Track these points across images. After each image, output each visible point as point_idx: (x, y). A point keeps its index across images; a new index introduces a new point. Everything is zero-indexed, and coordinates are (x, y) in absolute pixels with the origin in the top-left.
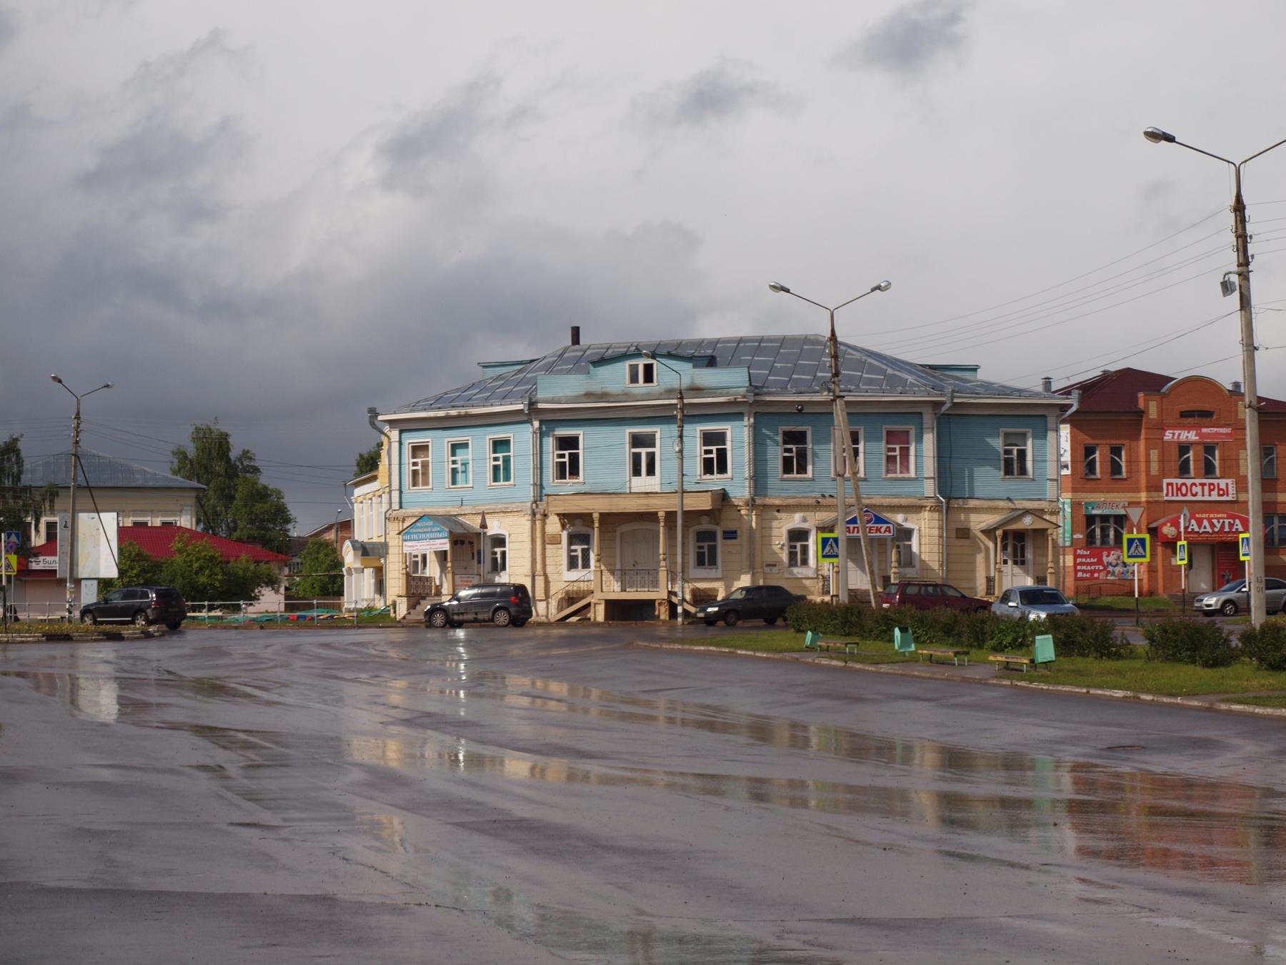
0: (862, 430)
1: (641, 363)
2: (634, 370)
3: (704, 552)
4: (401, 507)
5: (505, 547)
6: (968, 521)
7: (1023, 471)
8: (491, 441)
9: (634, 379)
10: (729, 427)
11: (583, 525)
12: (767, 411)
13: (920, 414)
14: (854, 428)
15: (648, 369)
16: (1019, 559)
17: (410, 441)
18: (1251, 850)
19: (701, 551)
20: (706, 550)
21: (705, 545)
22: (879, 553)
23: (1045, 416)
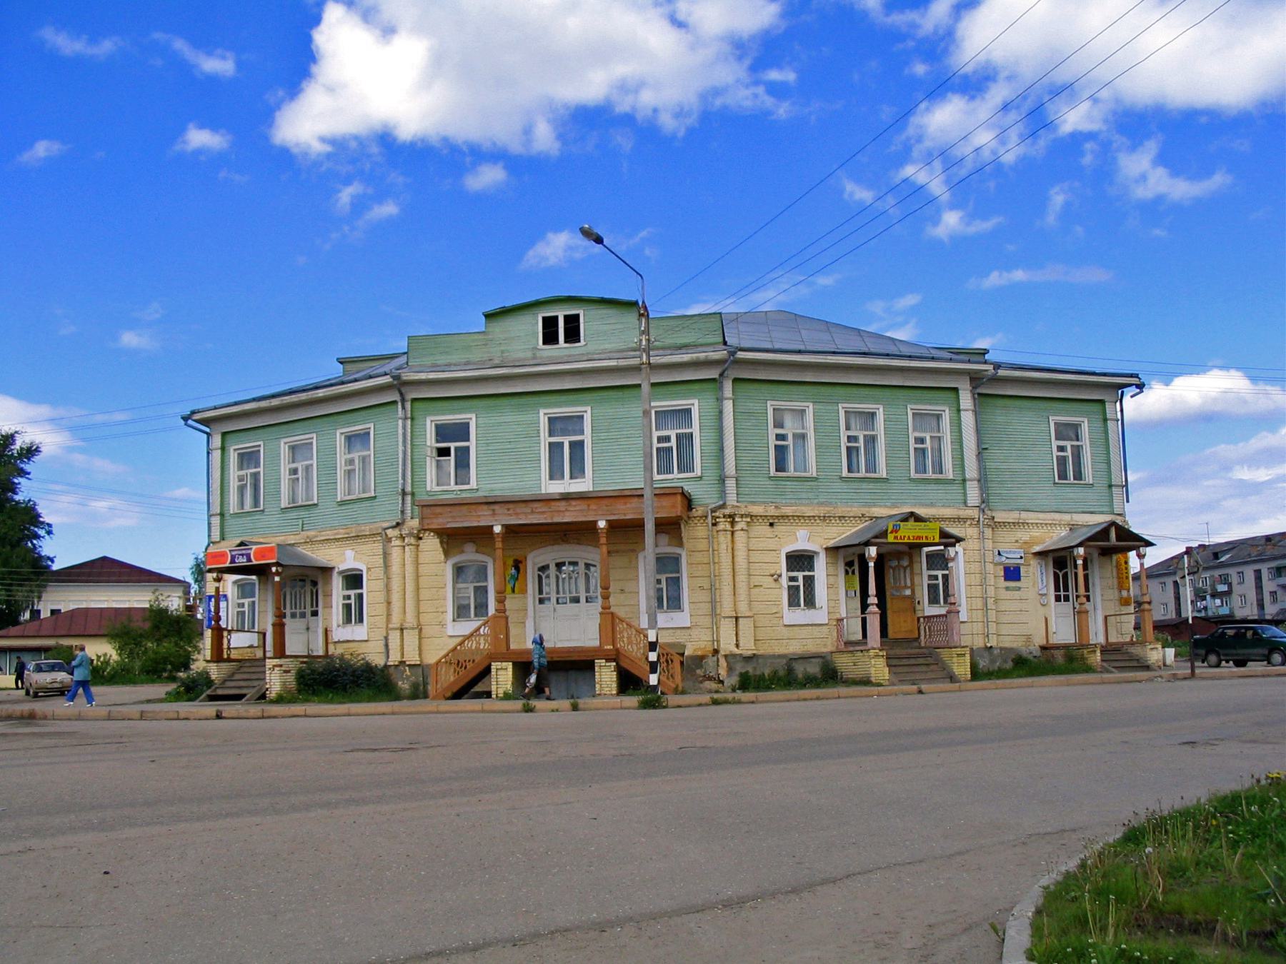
0: (881, 410)
1: (561, 313)
2: (550, 324)
3: (799, 586)
4: (223, 539)
5: (361, 587)
6: (113, 660)
7: (1078, 475)
8: (343, 437)
9: (550, 338)
10: (696, 402)
11: (477, 552)
12: (741, 377)
13: (956, 390)
14: (659, 577)
15: (572, 322)
16: (1062, 593)
17: (236, 447)
18: (800, 669)
19: (1062, 454)
20: (801, 582)
21: (800, 575)
22: (1100, 578)
23: (1102, 402)
